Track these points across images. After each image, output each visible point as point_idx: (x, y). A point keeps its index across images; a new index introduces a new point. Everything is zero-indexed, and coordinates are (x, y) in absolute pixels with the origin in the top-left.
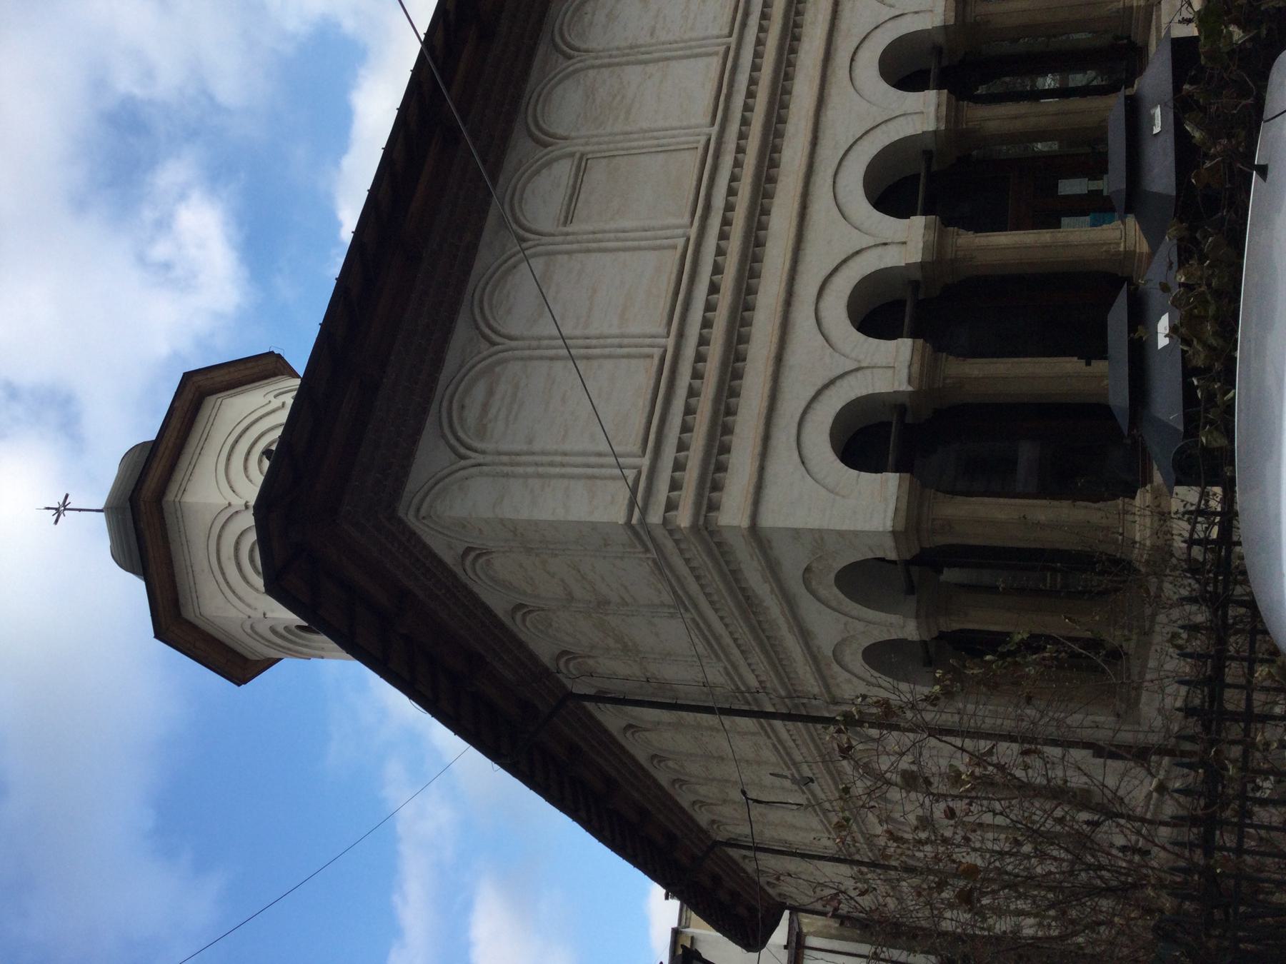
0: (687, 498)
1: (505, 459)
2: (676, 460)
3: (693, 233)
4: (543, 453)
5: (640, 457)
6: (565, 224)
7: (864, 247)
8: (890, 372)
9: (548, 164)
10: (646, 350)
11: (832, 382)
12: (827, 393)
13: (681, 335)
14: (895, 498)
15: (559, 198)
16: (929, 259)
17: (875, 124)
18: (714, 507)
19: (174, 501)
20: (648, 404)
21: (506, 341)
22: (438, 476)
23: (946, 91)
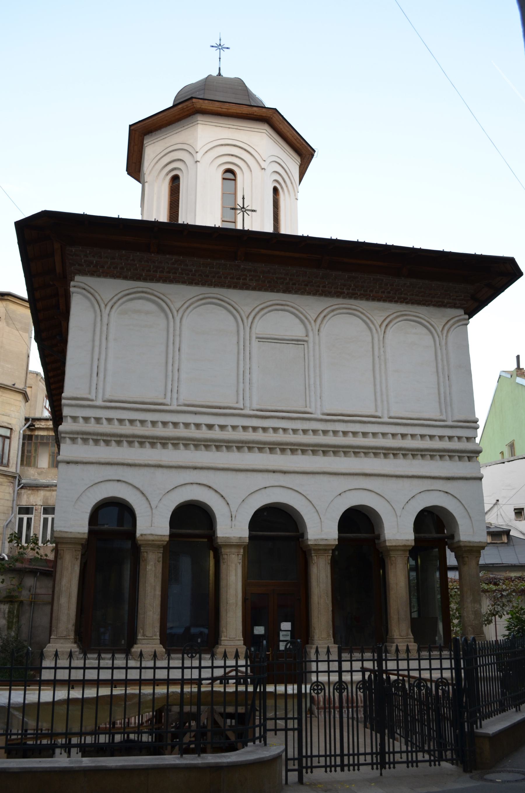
0: (81, 426)
2: (338, 431)
3: (247, 412)
5: (103, 399)
8: (150, 526)
12: (138, 493)
15: (281, 333)
16: (219, 541)
17: (315, 506)
18: (73, 440)
19: (198, 121)
22: (97, 295)
23: (337, 543)
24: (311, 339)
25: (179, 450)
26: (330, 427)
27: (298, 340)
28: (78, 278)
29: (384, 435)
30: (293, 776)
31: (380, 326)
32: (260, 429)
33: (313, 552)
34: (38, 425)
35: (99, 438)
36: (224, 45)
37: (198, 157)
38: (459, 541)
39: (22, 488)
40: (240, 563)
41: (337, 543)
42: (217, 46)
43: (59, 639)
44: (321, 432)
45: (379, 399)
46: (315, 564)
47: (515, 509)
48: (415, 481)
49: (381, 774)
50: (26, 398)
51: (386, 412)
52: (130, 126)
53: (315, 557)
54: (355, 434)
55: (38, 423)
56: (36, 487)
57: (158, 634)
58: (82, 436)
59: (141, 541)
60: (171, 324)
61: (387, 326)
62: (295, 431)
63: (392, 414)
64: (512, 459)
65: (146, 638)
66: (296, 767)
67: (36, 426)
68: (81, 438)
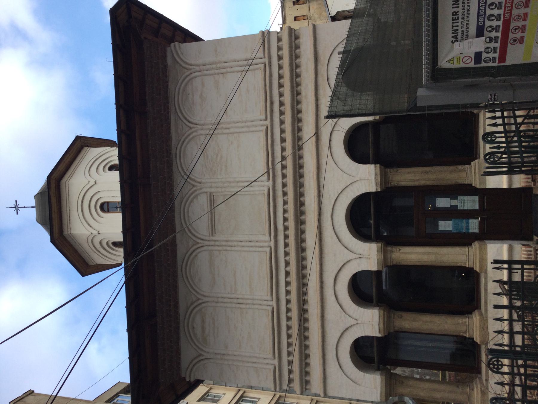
3: (272, 244)
6: (213, 235)
7: (352, 324)
9: (196, 196)
11: (347, 329)
12: (345, 333)
13: (278, 299)
14: (380, 387)
19: (68, 234)
20: (271, 335)
21: (202, 242)
24: (208, 190)
25: (308, 300)
26: (281, 227)
27: (211, 201)
29: (282, 122)
33: (387, 186)
36: (14, 205)
37: (95, 232)
40: (400, 250)
41: (378, 165)
42: (16, 210)
43: (470, 400)
44: (284, 180)
46: (398, 183)
51: (262, 123)
52: (83, 276)
53: (392, 183)
58: (304, 376)
59: (384, 333)
61: (189, 122)
65: (468, 331)
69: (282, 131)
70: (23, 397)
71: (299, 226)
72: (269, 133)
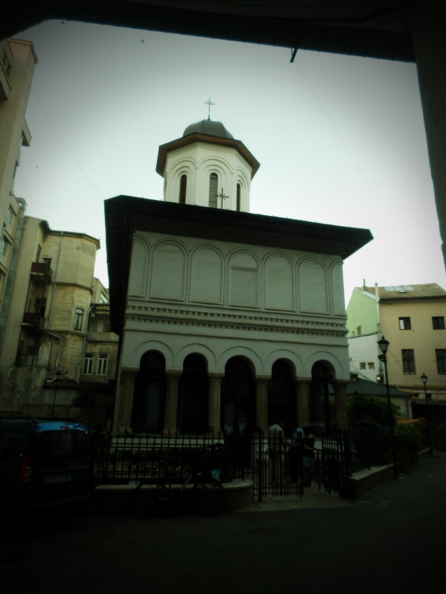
0: (137, 311)
1: (151, 260)
3: (225, 306)
4: (152, 270)
7: (174, 353)
10: (184, 296)
11: (170, 349)
18: (133, 319)
21: (228, 259)
22: (147, 242)
26: (235, 313)
28: (137, 232)
29: (297, 321)
30: (256, 498)
31: (297, 263)
32: (232, 316)
34: (98, 308)
35: (147, 318)
37: (198, 166)
38: (336, 379)
39: (88, 343)
44: (264, 319)
45: (295, 302)
47: (361, 363)
48: (313, 347)
49: (301, 499)
50: (92, 293)
54: (282, 320)
55: (98, 307)
56: (95, 342)
57: (176, 424)
60: (186, 258)
62: (250, 318)
63: (302, 311)
64: (360, 335)
66: (258, 493)
67: (97, 309)
68: (137, 318)
69: (292, 321)
70: (34, 54)
71: (236, 325)
72: (292, 313)
